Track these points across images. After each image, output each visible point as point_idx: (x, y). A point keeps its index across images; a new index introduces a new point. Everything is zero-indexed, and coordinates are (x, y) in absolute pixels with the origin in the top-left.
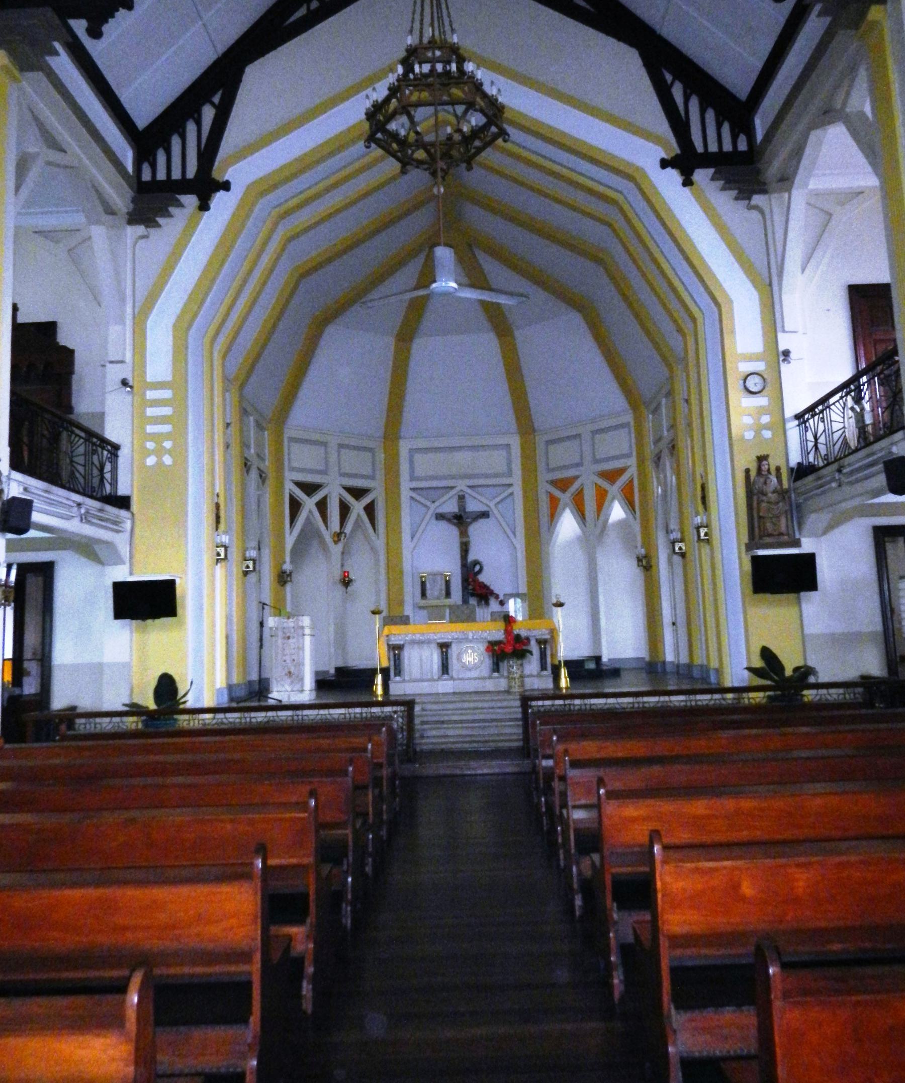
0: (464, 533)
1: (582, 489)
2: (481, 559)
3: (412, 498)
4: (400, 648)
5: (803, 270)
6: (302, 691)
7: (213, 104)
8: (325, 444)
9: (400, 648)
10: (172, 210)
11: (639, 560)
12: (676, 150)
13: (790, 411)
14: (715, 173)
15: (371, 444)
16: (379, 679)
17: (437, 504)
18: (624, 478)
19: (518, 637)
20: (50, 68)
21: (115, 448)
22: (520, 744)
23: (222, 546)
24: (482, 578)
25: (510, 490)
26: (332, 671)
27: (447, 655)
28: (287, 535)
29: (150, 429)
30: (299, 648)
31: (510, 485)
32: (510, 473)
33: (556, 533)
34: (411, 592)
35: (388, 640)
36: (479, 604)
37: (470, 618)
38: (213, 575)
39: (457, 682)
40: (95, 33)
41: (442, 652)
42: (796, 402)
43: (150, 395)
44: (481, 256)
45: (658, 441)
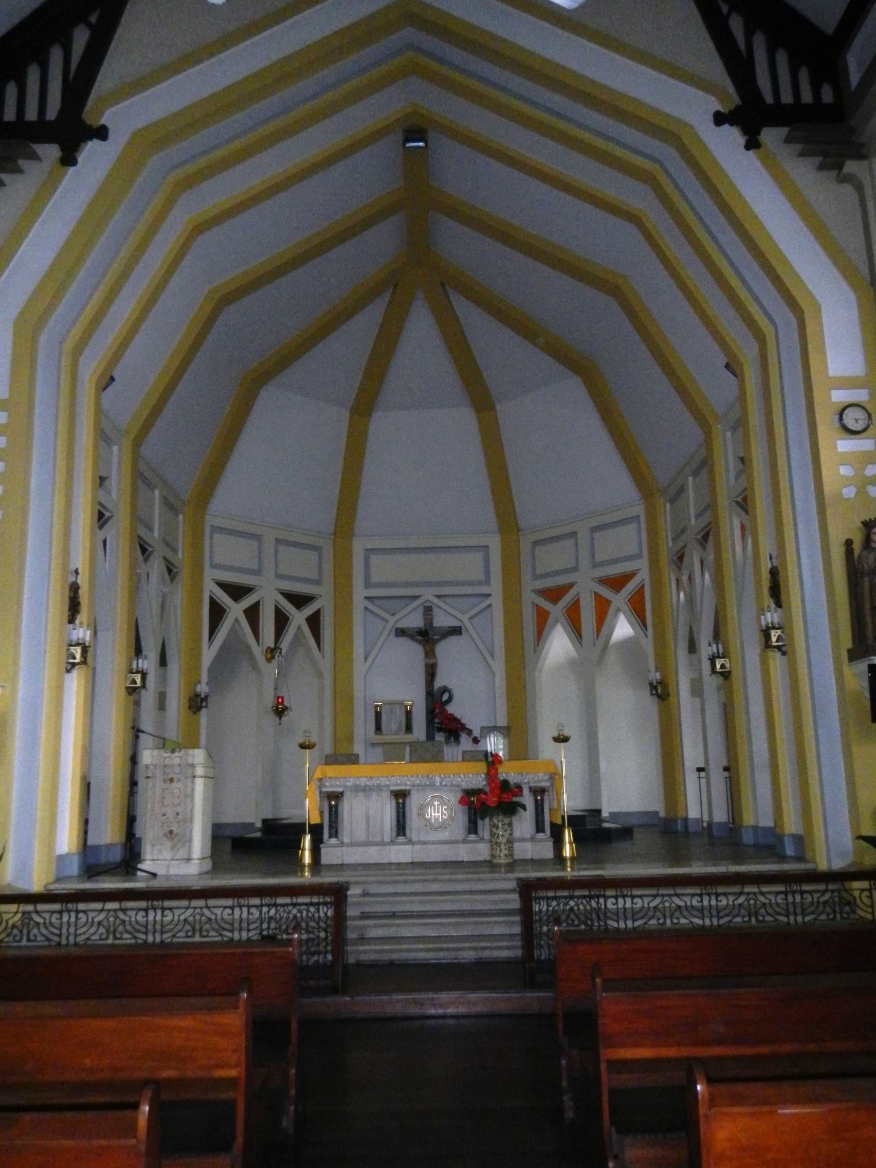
0: (430, 654)
3: (366, 609)
4: (337, 797)
6: (189, 859)
7: (89, 25)
9: (337, 797)
11: (653, 687)
12: (734, 99)
16: (307, 840)
18: (631, 587)
19: (505, 783)
22: (519, 953)
23: (78, 644)
24: (451, 709)
25: (487, 602)
26: (259, 824)
27: (404, 807)
30: (186, 796)
31: (490, 595)
32: (487, 581)
33: (544, 651)
34: (363, 727)
35: (320, 787)
36: (447, 742)
37: (437, 758)
38: (59, 689)
39: (418, 847)
41: (398, 804)
45: (679, 534)
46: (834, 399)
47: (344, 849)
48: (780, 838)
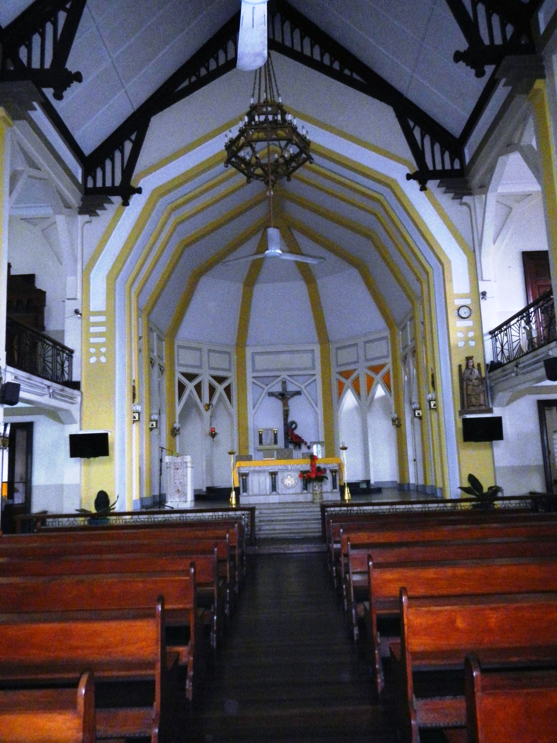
0: (285, 404)
1: (358, 378)
2: (296, 420)
3: (254, 383)
4: (246, 475)
5: (494, 242)
6: (186, 502)
7: (131, 140)
8: (200, 350)
9: (246, 475)
10: (106, 205)
11: (393, 421)
13: (486, 330)
14: (440, 182)
15: (228, 350)
16: (233, 494)
17: (269, 386)
18: (384, 370)
19: (319, 468)
20: (31, 118)
21: (71, 352)
22: (320, 534)
23: (137, 412)
24: (297, 432)
25: (314, 378)
26: (205, 489)
27: (275, 479)
28: (177, 406)
29: (92, 340)
30: (184, 475)
31: (314, 375)
32: (314, 368)
33: (342, 404)
34: (253, 440)
35: (239, 471)
36: (295, 448)
39: (281, 496)
40: (59, 96)
41: (272, 478)
42: (490, 324)
43: (93, 319)
44: (296, 234)
45: (405, 348)
46: (456, 304)
47: (250, 497)
48: (436, 489)
